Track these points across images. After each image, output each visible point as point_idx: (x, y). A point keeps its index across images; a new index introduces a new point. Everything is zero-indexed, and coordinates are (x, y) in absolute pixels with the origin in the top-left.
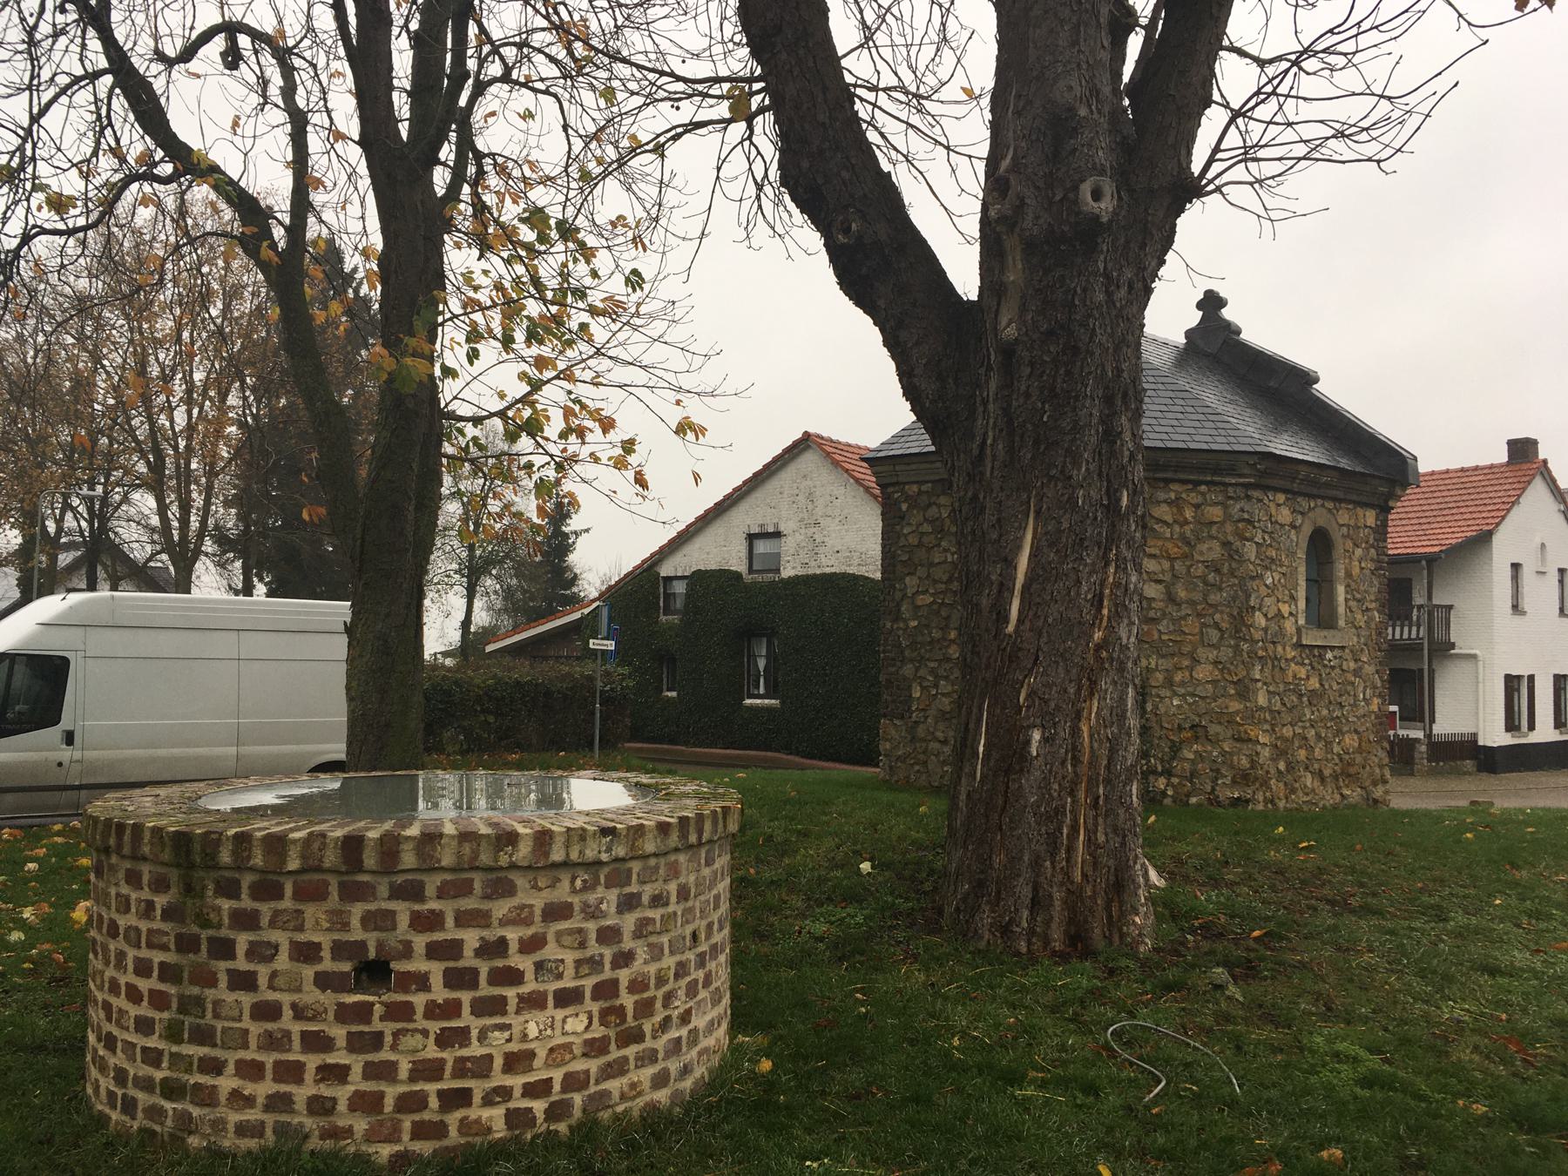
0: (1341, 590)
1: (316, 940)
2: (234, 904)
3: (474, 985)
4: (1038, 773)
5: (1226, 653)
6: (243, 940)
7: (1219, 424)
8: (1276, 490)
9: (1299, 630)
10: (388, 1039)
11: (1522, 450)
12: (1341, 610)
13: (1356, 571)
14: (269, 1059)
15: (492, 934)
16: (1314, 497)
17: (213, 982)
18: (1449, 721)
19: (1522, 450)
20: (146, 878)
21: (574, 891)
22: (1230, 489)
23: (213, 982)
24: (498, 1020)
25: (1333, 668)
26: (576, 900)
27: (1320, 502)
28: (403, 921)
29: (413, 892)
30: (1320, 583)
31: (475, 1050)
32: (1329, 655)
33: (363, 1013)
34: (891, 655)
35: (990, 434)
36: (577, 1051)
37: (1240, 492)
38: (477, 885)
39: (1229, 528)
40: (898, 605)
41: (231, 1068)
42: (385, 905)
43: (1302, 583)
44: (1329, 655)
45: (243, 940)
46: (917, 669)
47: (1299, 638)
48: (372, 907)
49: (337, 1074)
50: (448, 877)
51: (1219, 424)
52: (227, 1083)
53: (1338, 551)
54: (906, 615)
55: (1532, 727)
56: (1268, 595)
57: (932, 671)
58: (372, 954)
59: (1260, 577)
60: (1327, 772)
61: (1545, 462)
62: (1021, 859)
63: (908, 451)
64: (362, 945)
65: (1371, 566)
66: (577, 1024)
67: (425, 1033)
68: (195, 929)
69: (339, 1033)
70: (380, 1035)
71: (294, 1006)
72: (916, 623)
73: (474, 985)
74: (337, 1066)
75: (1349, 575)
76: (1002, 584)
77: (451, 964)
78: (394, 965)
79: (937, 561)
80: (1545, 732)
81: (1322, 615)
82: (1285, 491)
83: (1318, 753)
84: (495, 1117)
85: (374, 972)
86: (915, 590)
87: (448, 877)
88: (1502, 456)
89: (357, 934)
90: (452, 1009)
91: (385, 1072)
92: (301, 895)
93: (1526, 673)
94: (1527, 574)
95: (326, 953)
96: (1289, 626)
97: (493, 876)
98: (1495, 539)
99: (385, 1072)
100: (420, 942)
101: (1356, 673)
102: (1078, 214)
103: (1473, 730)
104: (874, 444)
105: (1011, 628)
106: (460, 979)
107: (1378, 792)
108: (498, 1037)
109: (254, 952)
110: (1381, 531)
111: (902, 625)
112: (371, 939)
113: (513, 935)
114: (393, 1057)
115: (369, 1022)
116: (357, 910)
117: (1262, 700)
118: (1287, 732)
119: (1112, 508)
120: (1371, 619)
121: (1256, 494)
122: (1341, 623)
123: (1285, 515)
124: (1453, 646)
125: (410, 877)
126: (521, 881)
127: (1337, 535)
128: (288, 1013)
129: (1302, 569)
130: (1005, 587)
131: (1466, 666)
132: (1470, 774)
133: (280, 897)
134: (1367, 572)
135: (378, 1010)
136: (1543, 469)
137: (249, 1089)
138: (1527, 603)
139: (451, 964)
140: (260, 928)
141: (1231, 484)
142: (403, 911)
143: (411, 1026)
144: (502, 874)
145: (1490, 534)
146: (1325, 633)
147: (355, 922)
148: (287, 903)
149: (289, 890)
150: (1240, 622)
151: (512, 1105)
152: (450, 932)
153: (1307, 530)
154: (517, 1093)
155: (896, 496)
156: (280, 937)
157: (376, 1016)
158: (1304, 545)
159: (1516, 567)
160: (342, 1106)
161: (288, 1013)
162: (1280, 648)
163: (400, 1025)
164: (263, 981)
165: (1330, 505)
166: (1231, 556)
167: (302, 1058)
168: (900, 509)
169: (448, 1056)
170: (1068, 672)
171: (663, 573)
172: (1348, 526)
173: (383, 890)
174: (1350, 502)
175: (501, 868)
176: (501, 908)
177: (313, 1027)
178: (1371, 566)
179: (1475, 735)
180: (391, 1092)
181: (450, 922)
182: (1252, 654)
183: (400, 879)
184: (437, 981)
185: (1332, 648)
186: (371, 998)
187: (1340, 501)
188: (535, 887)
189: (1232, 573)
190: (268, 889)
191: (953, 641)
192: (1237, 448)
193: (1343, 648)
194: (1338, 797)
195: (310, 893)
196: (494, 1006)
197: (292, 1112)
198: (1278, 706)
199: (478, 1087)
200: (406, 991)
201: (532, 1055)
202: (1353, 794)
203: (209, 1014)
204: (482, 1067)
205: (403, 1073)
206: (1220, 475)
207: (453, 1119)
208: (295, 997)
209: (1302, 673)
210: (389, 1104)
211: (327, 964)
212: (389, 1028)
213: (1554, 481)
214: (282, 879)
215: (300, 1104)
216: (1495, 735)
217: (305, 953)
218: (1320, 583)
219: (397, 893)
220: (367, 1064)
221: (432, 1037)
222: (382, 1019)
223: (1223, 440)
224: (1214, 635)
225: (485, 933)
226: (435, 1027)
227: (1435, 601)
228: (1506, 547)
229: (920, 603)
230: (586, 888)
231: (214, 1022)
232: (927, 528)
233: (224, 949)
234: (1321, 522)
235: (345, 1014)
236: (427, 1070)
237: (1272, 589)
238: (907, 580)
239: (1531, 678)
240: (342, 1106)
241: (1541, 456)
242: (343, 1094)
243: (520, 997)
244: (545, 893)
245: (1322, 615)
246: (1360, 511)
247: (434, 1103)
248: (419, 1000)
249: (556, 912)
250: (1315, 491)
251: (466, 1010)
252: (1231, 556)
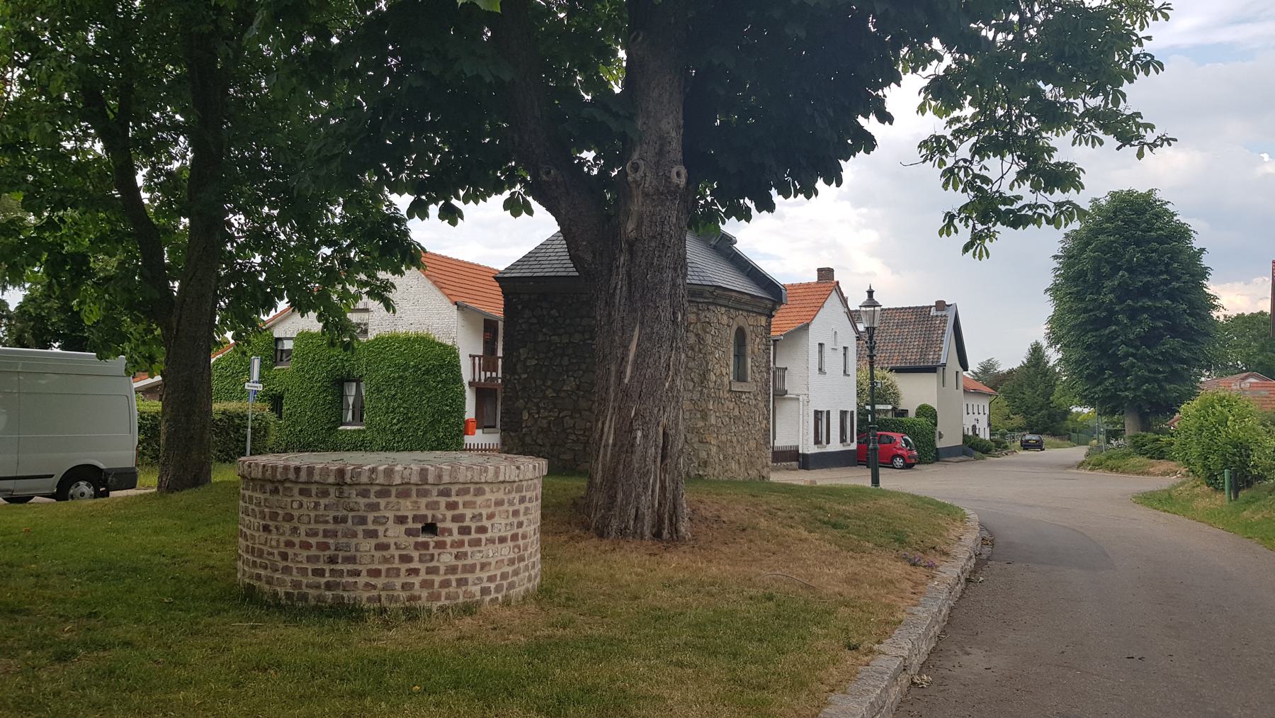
0: (749, 360)
1: (406, 514)
2: (366, 500)
3: (469, 533)
4: (640, 453)
5: (696, 396)
6: (371, 517)
7: (694, 269)
8: (721, 306)
9: (730, 382)
10: (436, 557)
11: (826, 274)
12: (749, 372)
13: (756, 350)
14: (383, 567)
15: (476, 511)
16: (738, 309)
17: (355, 535)
18: (783, 440)
19: (826, 274)
20: (314, 492)
21: (505, 494)
22: (700, 305)
23: (355, 535)
24: (478, 548)
25: (745, 404)
26: (506, 498)
27: (741, 312)
28: (443, 505)
29: (446, 493)
30: (740, 356)
31: (469, 561)
32: (744, 397)
33: (425, 545)
34: (510, 394)
35: (620, 283)
36: (506, 563)
37: (705, 306)
38: (472, 490)
39: (699, 325)
40: (515, 365)
41: (364, 573)
42: (436, 499)
43: (732, 356)
44: (744, 397)
45: (371, 517)
46: (527, 403)
47: (730, 387)
48: (430, 500)
49: (415, 572)
50: (461, 486)
51: (694, 269)
52: (362, 580)
53: (748, 340)
54: (519, 371)
55: (828, 442)
56: (717, 363)
57: (537, 405)
58: (429, 521)
59: (712, 353)
60: (741, 461)
61: (838, 283)
62: (631, 496)
63: (524, 275)
64: (425, 517)
65: (763, 347)
66: (505, 551)
67: (451, 554)
68: (345, 513)
69: (416, 555)
70: (398, 570)
71: (396, 544)
72: (526, 376)
73: (469, 533)
74: (415, 569)
75: (753, 352)
76: (623, 358)
77: (461, 524)
78: (439, 525)
79: (540, 339)
80: (835, 446)
81: (740, 376)
82: (725, 306)
83: (738, 450)
84: (476, 589)
85: (430, 528)
86: (525, 356)
87: (461, 486)
88: (813, 278)
89: (423, 511)
90: (461, 544)
91: (433, 571)
92: (399, 495)
93: (825, 409)
94: (827, 349)
95: (410, 520)
96: (726, 380)
97: (478, 486)
98: (811, 327)
99: (434, 571)
100: (449, 514)
101: (755, 406)
102: (670, 183)
103: (795, 444)
104: (502, 268)
105: (626, 381)
106: (465, 531)
107: (764, 474)
108: (479, 555)
109: (376, 521)
110: (768, 328)
111: (517, 377)
112: (429, 513)
113: (484, 512)
114: (438, 564)
115: (428, 549)
116: (423, 501)
117: (713, 421)
118: (724, 438)
119: (674, 322)
120: (763, 377)
121: (711, 307)
122: (749, 379)
123: (725, 320)
124: (786, 392)
125: (446, 486)
126: (487, 488)
127: (748, 330)
128: (393, 547)
129: (732, 349)
130: (624, 358)
131: (793, 404)
132: (795, 470)
133: (390, 496)
134: (761, 351)
135: (432, 544)
136: (837, 287)
137: (373, 581)
138: (826, 368)
139: (461, 524)
140: (380, 510)
141: (701, 303)
142: (443, 501)
143: (445, 551)
144: (480, 486)
145: (808, 325)
146: (743, 384)
147: (423, 506)
148: (393, 499)
149: (414, 493)
150: (704, 377)
151: (483, 585)
152: (461, 510)
153: (735, 327)
154: (485, 580)
155: (514, 300)
156: (390, 515)
157: (431, 547)
158: (733, 335)
159: (821, 345)
160: (417, 586)
161: (393, 547)
162: (721, 392)
163: (440, 551)
164: (381, 534)
165: (745, 314)
166: (699, 342)
167: (399, 566)
168: (517, 308)
169: (460, 563)
170: (654, 402)
171: (276, 335)
172: (753, 326)
173: (435, 493)
174: (755, 312)
175: (482, 483)
176: (479, 500)
177: (404, 552)
178: (763, 347)
179: (797, 447)
180: (437, 579)
181: (461, 506)
182: (709, 395)
183: (442, 487)
184: (455, 531)
185: (745, 393)
186: (429, 540)
187: (750, 311)
188: (492, 491)
189: (700, 351)
190: (384, 493)
191: (549, 387)
192: (704, 283)
193: (750, 392)
194: (746, 474)
195: (404, 494)
196: (477, 543)
197: (394, 590)
198: (720, 425)
199: (470, 577)
200: (443, 535)
201: (490, 564)
202: (753, 473)
203: (353, 550)
204: (472, 569)
205: (442, 571)
206: (696, 297)
207: (461, 591)
208: (396, 540)
209: (731, 406)
210: (436, 585)
211: (410, 525)
212: (436, 552)
213: (842, 294)
214: (391, 488)
215: (398, 586)
216: (809, 448)
217: (401, 520)
218: (740, 356)
219: (441, 494)
220: (428, 568)
221: (453, 555)
222: (434, 548)
223: (697, 278)
224: (691, 385)
225: (474, 511)
226: (455, 551)
227: (777, 366)
228: (817, 332)
229: (528, 364)
230: (510, 492)
231: (356, 553)
232: (535, 321)
233: (363, 521)
234: (741, 324)
235: (417, 546)
236: (452, 570)
237: (719, 360)
238: (521, 351)
239: (828, 412)
240: (417, 586)
241: (836, 279)
242: (416, 581)
243: (487, 540)
244: (496, 494)
245: (740, 376)
246: (759, 317)
247: (454, 584)
248: (448, 540)
249: (499, 503)
250: (738, 306)
251: (466, 544)
252: (699, 342)
